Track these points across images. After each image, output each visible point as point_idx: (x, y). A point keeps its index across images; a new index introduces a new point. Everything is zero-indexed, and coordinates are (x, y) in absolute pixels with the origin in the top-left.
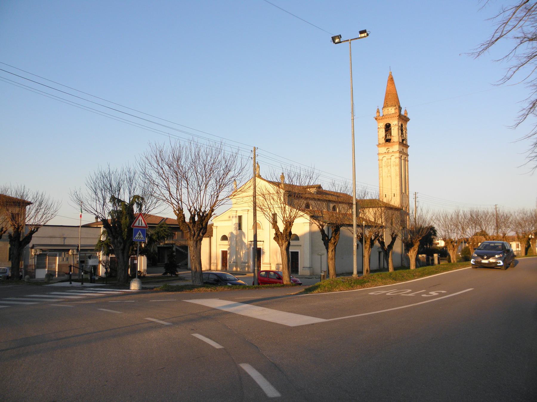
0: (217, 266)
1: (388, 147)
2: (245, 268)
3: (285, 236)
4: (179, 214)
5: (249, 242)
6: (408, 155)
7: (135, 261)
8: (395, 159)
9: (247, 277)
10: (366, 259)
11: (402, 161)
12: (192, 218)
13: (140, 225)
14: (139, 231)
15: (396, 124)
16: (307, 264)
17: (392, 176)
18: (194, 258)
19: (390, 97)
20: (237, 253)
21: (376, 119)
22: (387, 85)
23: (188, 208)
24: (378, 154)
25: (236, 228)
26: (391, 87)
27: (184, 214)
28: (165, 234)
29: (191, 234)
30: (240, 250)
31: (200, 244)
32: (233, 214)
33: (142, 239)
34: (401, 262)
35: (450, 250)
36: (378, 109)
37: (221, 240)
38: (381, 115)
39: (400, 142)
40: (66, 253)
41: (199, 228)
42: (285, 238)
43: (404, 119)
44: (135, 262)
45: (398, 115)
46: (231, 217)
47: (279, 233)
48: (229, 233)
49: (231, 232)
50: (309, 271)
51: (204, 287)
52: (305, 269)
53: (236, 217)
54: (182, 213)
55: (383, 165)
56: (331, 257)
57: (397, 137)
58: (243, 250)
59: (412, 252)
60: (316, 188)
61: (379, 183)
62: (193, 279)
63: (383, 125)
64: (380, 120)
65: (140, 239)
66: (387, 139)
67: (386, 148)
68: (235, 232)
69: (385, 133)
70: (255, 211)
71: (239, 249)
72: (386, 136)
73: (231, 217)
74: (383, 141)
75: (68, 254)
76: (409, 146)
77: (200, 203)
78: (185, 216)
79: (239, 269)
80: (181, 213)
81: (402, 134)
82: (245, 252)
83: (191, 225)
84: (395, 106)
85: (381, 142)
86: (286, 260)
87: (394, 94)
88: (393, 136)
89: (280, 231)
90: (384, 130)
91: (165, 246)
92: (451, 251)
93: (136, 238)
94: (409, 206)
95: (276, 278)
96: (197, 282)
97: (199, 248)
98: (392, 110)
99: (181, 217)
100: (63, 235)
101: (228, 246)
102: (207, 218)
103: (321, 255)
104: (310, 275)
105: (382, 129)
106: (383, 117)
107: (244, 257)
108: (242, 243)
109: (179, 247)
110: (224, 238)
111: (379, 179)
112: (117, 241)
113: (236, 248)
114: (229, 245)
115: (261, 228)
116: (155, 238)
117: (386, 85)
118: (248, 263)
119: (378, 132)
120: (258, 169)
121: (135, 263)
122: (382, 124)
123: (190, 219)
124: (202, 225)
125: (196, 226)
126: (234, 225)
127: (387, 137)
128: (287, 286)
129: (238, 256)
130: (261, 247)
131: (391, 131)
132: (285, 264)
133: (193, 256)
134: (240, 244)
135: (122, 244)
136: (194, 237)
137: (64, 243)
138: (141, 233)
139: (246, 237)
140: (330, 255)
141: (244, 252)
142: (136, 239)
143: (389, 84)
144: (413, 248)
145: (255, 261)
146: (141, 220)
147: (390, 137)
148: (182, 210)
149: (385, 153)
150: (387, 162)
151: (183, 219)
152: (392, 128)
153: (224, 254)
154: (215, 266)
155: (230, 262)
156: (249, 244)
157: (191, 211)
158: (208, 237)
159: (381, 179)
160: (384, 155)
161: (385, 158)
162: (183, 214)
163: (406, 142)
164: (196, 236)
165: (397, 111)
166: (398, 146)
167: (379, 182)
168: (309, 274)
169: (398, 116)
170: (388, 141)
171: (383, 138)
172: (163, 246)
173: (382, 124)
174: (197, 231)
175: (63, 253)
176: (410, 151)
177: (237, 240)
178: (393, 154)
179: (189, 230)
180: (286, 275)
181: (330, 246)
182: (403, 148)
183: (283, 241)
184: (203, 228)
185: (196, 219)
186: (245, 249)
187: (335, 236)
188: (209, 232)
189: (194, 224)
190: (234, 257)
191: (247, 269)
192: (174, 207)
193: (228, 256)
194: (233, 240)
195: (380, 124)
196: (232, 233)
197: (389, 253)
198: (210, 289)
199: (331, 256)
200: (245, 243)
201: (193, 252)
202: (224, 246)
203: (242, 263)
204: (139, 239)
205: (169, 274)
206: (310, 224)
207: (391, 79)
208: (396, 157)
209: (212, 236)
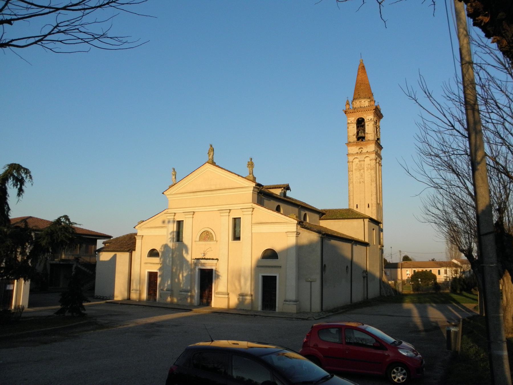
0: (140, 294)
1: (361, 146)
2: (187, 299)
5: (193, 260)
6: (381, 159)
7: (8, 286)
8: (369, 161)
15: (371, 119)
16: (292, 295)
17: (366, 182)
19: (362, 87)
20: (173, 276)
21: (346, 112)
22: (358, 74)
24: (347, 154)
25: (173, 238)
28: (66, 237)
30: (178, 271)
32: (168, 217)
34: (379, 290)
36: (348, 101)
43: (378, 114)
46: (166, 222)
48: (161, 244)
49: (165, 243)
50: (295, 306)
52: (287, 303)
53: (174, 222)
55: (354, 168)
57: (373, 135)
58: (184, 271)
60: (283, 189)
61: (349, 191)
63: (355, 119)
64: (351, 114)
66: (358, 136)
67: (358, 148)
68: (171, 245)
69: (357, 129)
71: (176, 270)
72: (358, 133)
73: (166, 222)
74: (355, 139)
76: (382, 148)
79: (175, 300)
81: (377, 132)
85: (352, 141)
87: (366, 84)
91: (61, 263)
94: (383, 220)
98: (365, 103)
101: (159, 266)
103: (311, 282)
104: (297, 313)
105: (353, 125)
107: (184, 282)
108: (183, 260)
110: (153, 253)
111: (349, 185)
113: (172, 269)
114: (161, 264)
115: (215, 239)
116: (46, 244)
118: (190, 291)
119: (348, 128)
120: (212, 153)
121: (8, 288)
122: (353, 118)
126: (171, 234)
127: (359, 134)
129: (175, 281)
130: (214, 268)
134: (178, 262)
139: (190, 252)
141: (185, 274)
147: (363, 134)
149: (357, 153)
150: (360, 165)
152: (366, 124)
153: (152, 277)
154: (138, 294)
155: (162, 290)
156: (194, 262)
158: (128, 251)
159: (351, 185)
160: (356, 157)
161: (357, 161)
166: (374, 145)
167: (349, 189)
169: (374, 109)
170: (361, 138)
171: (354, 135)
172: (58, 262)
173: (353, 118)
177: (174, 256)
178: (367, 155)
186: (188, 270)
188: (129, 244)
190: (168, 282)
191: (189, 300)
193: (159, 280)
195: (350, 119)
196: (166, 246)
200: (187, 262)
202: (152, 265)
205: (67, 314)
206: (296, 234)
207: (362, 68)
208: (371, 158)
209: (134, 250)
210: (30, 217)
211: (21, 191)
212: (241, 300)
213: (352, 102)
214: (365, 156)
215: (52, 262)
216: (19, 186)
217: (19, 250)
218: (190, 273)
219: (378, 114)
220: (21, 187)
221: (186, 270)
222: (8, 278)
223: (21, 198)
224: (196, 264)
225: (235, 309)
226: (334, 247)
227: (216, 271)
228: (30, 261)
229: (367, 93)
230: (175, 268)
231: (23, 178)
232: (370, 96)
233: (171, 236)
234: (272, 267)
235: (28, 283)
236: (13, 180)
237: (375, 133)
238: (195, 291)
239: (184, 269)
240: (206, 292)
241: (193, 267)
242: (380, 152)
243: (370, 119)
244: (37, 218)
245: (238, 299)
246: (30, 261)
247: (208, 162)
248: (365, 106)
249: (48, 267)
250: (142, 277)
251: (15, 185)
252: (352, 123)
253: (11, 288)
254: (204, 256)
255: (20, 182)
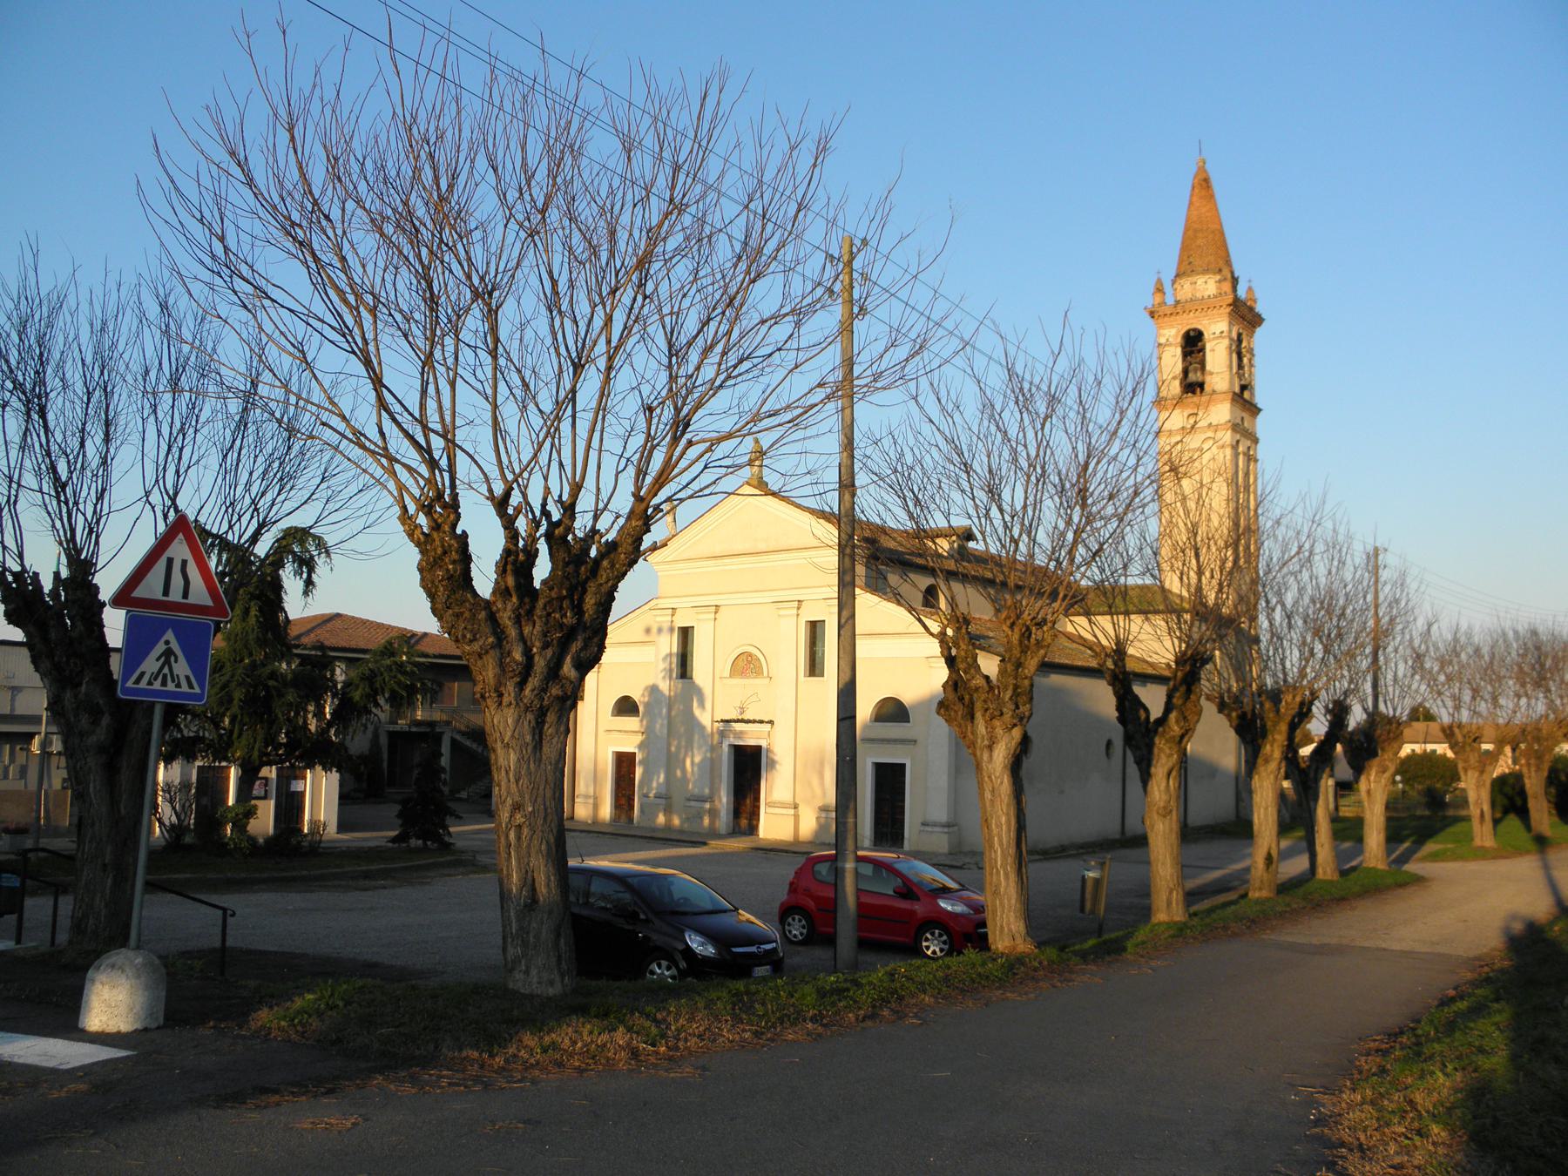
0: (596, 807)
3: (1011, 699)
4: (435, 535)
6: (1256, 441)
7: (294, 782)
9: (709, 855)
10: (1266, 808)
11: (1241, 457)
12: (516, 562)
13: (175, 595)
14: (164, 632)
16: (940, 813)
18: (519, 819)
19: (1199, 242)
20: (672, 762)
21: (1152, 314)
22: (1191, 203)
23: (490, 490)
25: (671, 670)
26: (1204, 210)
27: (465, 535)
28: (399, 683)
29: (502, 665)
30: (683, 751)
31: (562, 728)
32: (658, 619)
33: (185, 688)
35: (1466, 770)
36: (1159, 281)
37: (613, 715)
38: (1170, 300)
39: (1235, 393)
40: (18, 747)
41: (561, 625)
42: (1008, 710)
43: (1246, 316)
44: (297, 786)
45: (1230, 301)
46: (654, 630)
47: (979, 681)
49: (651, 683)
50: (945, 837)
51: (582, 1010)
52: (929, 829)
53: (671, 630)
54: (454, 526)
56: (1162, 804)
57: (1227, 376)
58: (696, 751)
59: (1372, 778)
60: (954, 538)
62: (511, 951)
63: (1176, 336)
65: (171, 687)
68: (664, 686)
70: (847, 560)
71: (678, 748)
72: (1186, 372)
73: (654, 630)
74: (1176, 388)
75: (28, 750)
76: (1260, 410)
77: (569, 469)
78: (473, 548)
79: (676, 821)
80: (447, 528)
81: (1240, 366)
82: (702, 761)
83: (509, 606)
84: (1220, 270)
86: (1008, 821)
88: (1211, 374)
89: (985, 671)
90: (1179, 351)
91: (414, 729)
92: (1470, 773)
93: (138, 681)
95: (891, 893)
96: (534, 972)
97: (554, 756)
98: (1207, 286)
99: (445, 553)
100: (8, 678)
101: (639, 738)
102: (613, 566)
104: (951, 854)
105: (1172, 349)
106: (1179, 309)
108: (693, 724)
109: (463, 734)
110: (626, 706)
112: (76, 696)
113: (669, 745)
115: (765, 674)
116: (361, 697)
117: (1187, 203)
118: (710, 799)
121: (293, 789)
122: (1173, 331)
123: (502, 567)
124: (579, 610)
125: (538, 612)
126: (664, 659)
128: (1014, 963)
130: (763, 743)
131: (1204, 355)
132: (1001, 844)
133: (517, 807)
134: (682, 730)
135: (106, 720)
136: (521, 685)
137: (13, 709)
138: (175, 646)
139: (708, 705)
140: (1157, 793)
141: (697, 759)
142: (143, 684)
143: (1195, 199)
144: (1375, 762)
145: (845, 824)
146: (184, 563)
147: (1199, 374)
148: (454, 506)
151: (454, 562)
155: (646, 796)
157: (510, 511)
162: (459, 531)
163: (1252, 394)
164: (533, 682)
165: (1227, 287)
168: (946, 850)
170: (1192, 387)
171: (1174, 378)
172: (406, 728)
173: (1173, 331)
174: (545, 646)
175: (8, 747)
176: (1262, 425)
177: (673, 713)
179: (491, 640)
180: (1009, 901)
181: (1161, 749)
182: (1244, 415)
183: (997, 723)
184: (585, 628)
185: (542, 570)
186: (704, 749)
187: (1184, 703)
189: (527, 600)
191: (706, 821)
192: (401, 487)
193: (639, 771)
194: (660, 713)
196: (653, 689)
197: (1317, 780)
198: (621, 1036)
199: (1164, 797)
200: (703, 728)
201: (517, 782)
203: (689, 800)
204: (164, 683)
205: (415, 843)
207: (1204, 184)
210: (338, 615)
211: (309, 583)
212: (822, 821)
213: (1174, 282)
214: (1204, 437)
215: (392, 728)
216: (305, 576)
217: (311, 708)
218: (708, 755)
219: (1246, 316)
220: (309, 576)
221: (700, 747)
222: (292, 766)
223: (309, 599)
224: (722, 734)
225: (810, 843)
226: (1058, 691)
227: (768, 750)
228: (332, 731)
229: (1212, 258)
230: (675, 743)
231: (312, 557)
232: (1223, 265)
233: (666, 665)
234: (895, 741)
235: (335, 776)
236: (294, 562)
237: (1235, 370)
238: (720, 801)
239: (695, 745)
240: (748, 801)
241: (715, 742)
242: (1254, 425)
243: (1218, 332)
244: (353, 617)
245: (817, 818)
246: (332, 731)
247: (748, 483)
248: (1206, 294)
249: (384, 740)
250: (600, 767)
251: (298, 573)
252: (1170, 345)
253: (300, 788)
254: (742, 711)
255: (306, 565)
